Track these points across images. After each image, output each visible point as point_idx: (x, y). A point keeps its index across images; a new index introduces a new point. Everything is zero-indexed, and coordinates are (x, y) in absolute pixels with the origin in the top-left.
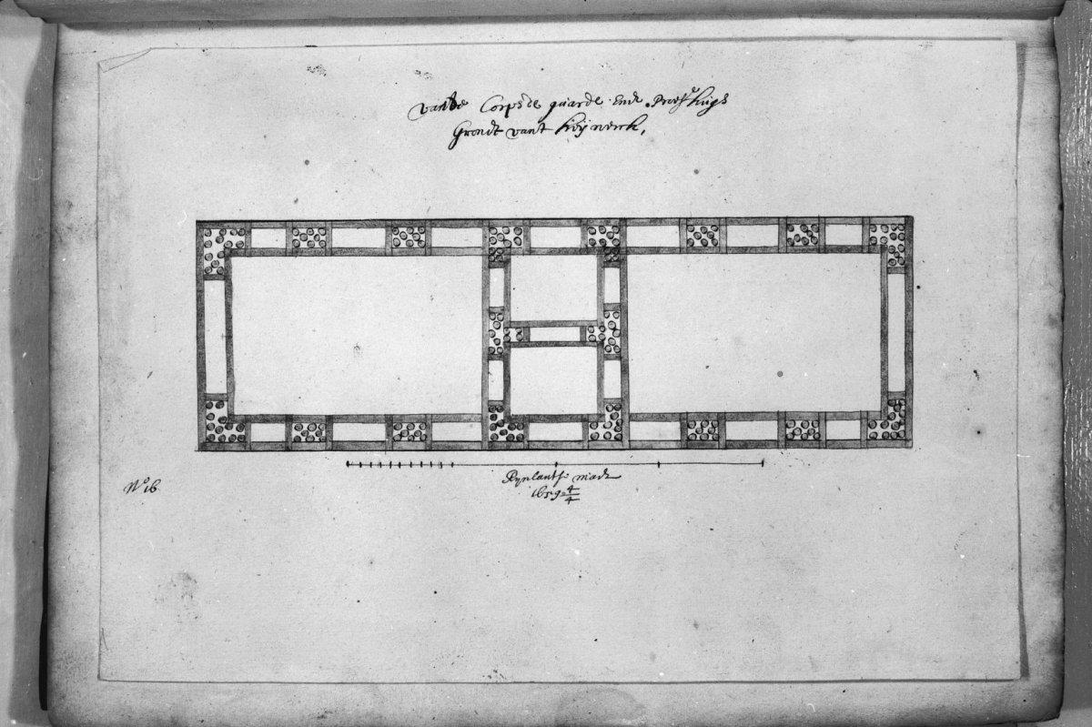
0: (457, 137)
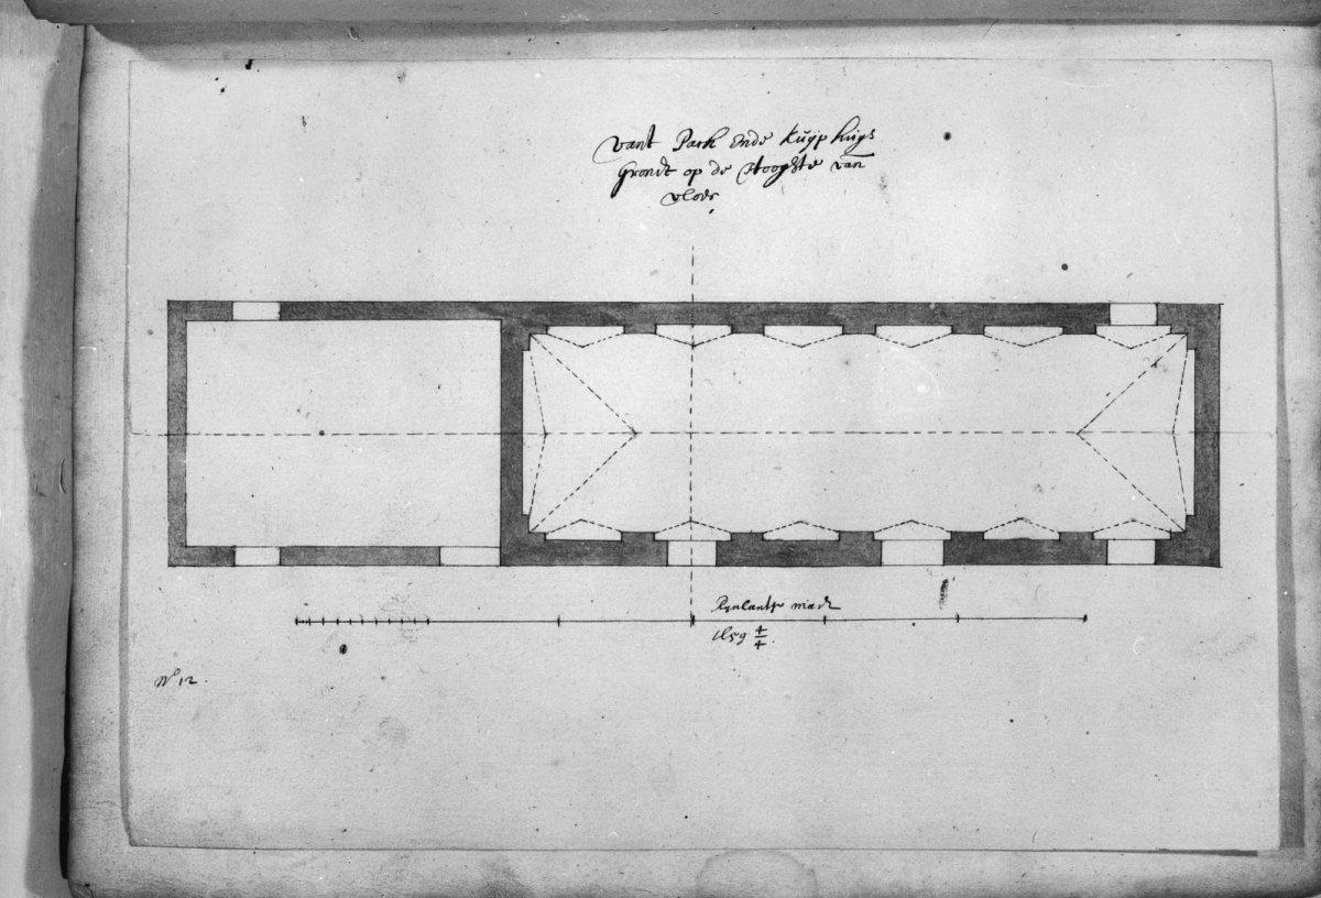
0: (622, 177)
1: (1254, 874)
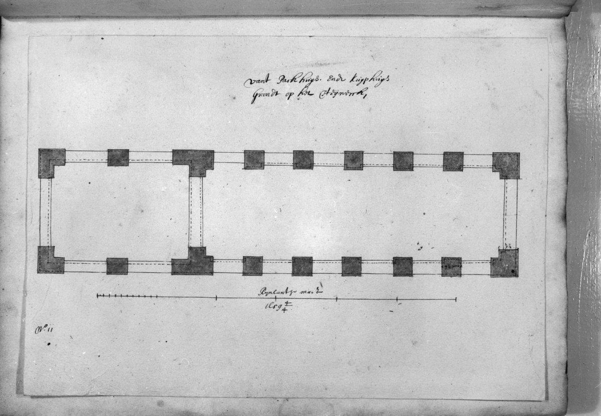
1: (535, 408)
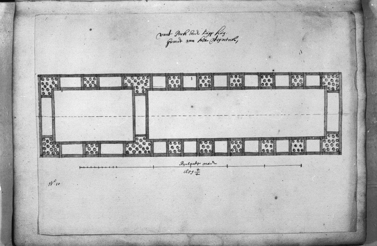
0: (168, 44)
